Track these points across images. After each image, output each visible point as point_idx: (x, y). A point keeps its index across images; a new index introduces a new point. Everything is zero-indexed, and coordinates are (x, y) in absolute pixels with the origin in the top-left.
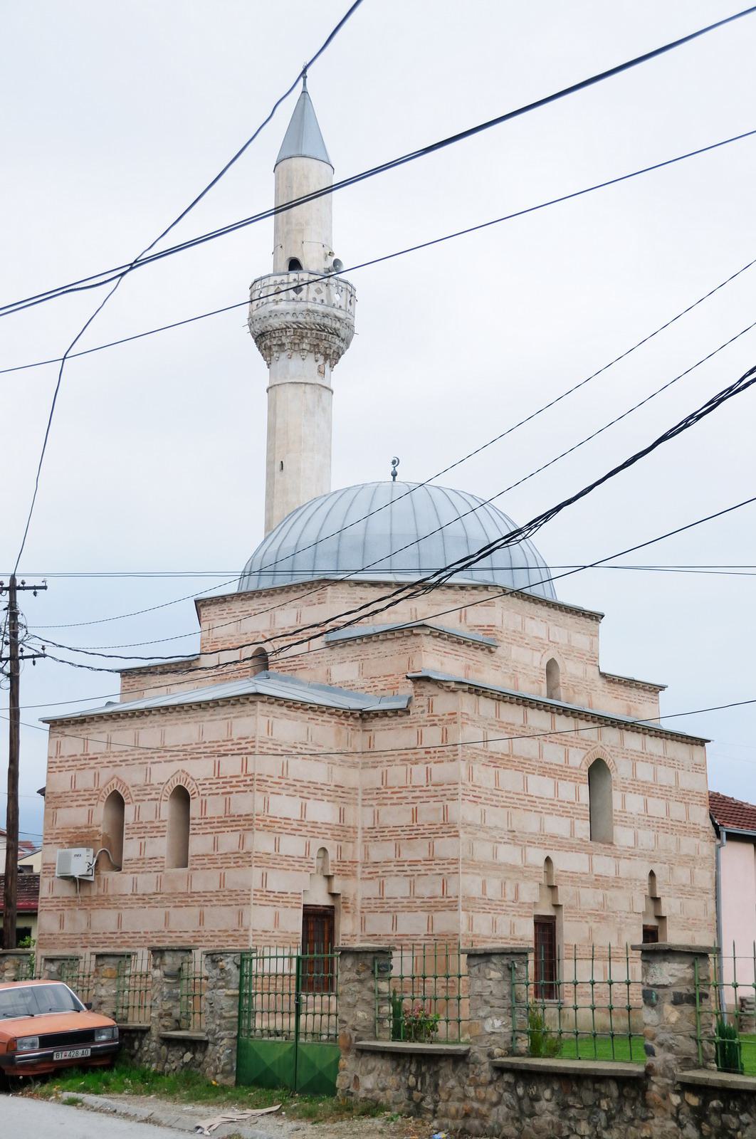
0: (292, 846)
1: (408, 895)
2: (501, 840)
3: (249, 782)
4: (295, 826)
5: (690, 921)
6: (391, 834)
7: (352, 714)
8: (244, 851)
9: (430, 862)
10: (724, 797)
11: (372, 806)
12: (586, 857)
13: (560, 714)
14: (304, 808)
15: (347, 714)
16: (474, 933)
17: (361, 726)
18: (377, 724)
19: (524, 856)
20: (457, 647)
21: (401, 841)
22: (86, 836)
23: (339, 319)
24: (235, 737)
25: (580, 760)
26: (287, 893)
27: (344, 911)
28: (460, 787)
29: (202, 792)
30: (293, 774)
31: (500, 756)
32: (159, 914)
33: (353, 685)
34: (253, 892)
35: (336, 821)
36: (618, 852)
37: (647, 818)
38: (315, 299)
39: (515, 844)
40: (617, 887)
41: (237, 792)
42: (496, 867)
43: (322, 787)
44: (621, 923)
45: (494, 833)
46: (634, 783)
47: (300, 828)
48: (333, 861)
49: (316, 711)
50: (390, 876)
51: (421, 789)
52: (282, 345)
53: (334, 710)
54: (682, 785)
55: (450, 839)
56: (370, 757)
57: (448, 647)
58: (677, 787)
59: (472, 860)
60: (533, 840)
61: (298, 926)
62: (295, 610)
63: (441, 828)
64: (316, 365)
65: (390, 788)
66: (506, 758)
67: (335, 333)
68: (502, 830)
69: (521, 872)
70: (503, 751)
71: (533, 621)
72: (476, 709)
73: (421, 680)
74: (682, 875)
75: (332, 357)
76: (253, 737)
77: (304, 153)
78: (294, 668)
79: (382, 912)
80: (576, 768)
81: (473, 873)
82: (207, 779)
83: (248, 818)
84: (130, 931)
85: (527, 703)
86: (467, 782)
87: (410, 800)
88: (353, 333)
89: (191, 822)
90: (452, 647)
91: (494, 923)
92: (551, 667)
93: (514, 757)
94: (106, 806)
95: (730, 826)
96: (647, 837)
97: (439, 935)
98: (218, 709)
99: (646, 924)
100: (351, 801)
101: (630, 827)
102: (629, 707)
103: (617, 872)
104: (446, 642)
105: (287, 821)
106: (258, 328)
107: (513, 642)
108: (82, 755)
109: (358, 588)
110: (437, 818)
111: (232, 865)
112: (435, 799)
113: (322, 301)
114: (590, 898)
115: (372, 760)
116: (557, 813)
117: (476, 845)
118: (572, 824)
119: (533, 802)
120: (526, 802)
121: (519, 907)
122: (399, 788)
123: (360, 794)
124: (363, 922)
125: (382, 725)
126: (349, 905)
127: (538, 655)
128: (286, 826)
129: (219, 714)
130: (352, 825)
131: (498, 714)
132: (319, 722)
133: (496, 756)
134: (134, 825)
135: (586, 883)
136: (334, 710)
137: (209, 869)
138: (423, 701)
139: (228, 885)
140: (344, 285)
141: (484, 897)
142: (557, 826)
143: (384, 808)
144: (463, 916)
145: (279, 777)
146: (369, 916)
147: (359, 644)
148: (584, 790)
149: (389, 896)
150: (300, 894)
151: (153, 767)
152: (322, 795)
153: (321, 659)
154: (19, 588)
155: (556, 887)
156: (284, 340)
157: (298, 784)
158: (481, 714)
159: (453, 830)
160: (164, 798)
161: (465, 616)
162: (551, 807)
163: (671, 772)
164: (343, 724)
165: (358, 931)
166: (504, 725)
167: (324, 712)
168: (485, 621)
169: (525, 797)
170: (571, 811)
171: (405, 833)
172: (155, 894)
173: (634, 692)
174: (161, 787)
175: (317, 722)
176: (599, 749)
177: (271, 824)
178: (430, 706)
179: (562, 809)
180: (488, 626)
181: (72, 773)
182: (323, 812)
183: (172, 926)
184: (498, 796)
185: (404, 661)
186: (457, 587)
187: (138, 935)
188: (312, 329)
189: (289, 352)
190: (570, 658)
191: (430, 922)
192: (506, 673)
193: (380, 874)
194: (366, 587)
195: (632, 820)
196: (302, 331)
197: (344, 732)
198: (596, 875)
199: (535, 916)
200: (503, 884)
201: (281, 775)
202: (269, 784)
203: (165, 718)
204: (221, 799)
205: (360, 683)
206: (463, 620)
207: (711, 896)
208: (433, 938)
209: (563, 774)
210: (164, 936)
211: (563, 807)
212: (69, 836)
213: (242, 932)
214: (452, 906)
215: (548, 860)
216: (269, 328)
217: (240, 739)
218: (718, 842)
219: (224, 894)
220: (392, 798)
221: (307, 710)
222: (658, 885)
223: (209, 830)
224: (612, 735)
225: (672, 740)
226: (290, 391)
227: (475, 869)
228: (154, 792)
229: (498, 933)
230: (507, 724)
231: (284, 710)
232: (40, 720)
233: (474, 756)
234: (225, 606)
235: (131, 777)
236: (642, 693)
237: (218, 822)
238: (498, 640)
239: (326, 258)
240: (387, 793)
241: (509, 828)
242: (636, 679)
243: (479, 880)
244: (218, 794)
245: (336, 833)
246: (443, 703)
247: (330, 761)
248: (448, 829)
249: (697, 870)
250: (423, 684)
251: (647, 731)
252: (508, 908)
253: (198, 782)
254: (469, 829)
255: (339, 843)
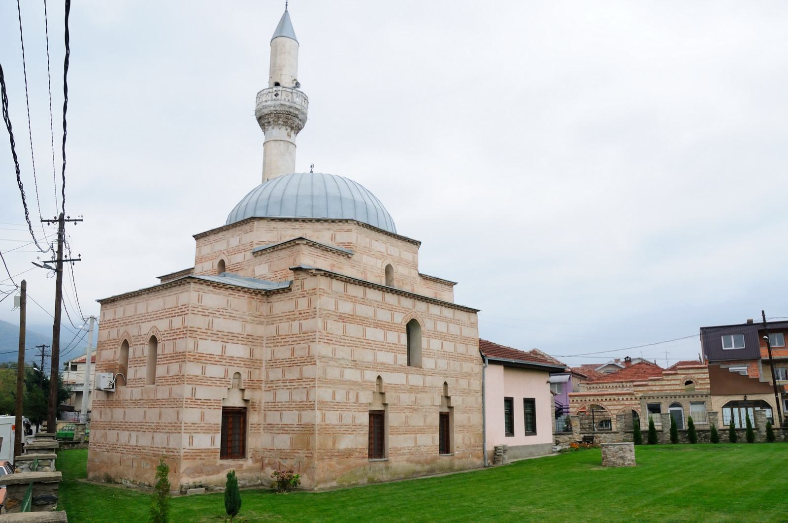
0: (215, 371)
1: (288, 400)
2: (346, 366)
3: (188, 332)
4: (217, 359)
5: (468, 408)
6: (280, 363)
7: (259, 292)
8: (181, 374)
9: (300, 380)
10: (491, 343)
11: (271, 347)
12: (404, 375)
13: (388, 292)
14: (224, 349)
15: (257, 292)
16: (326, 423)
17: (266, 300)
18: (274, 298)
19: (362, 376)
20: (325, 253)
21: (285, 368)
22: (112, 366)
23: (298, 109)
24: (180, 305)
25: (401, 320)
26: (210, 400)
27: (252, 410)
28: (318, 333)
29: (163, 339)
30: (216, 327)
31: (346, 316)
32: (141, 411)
33: (266, 277)
34: (185, 400)
35: (248, 356)
36: (425, 372)
37: (443, 353)
38: (285, 99)
39: (356, 369)
40: (424, 392)
41: (179, 338)
42: (342, 382)
43: (238, 335)
44: (426, 412)
45: (342, 362)
46: (435, 333)
47: (221, 360)
48: (245, 380)
49: (234, 290)
50: (279, 389)
51: (296, 336)
52: (269, 122)
53: (246, 290)
54: (464, 334)
55: (311, 366)
56: (271, 319)
57: (319, 252)
58: (461, 335)
59: (326, 379)
60: (369, 366)
61: (219, 420)
62: (239, 237)
63: (307, 359)
64: (287, 132)
65: (280, 336)
66: (351, 317)
67: (296, 116)
68: (348, 360)
69: (361, 385)
70: (349, 313)
71: (377, 243)
72: (330, 287)
73: (298, 270)
74: (463, 383)
75: (298, 129)
76: (188, 304)
77: (283, 35)
78: (237, 269)
79: (275, 411)
80: (398, 324)
81: (326, 387)
82: (165, 331)
83: (183, 354)
84: (129, 421)
85: (366, 285)
86: (323, 331)
87: (291, 343)
88: (307, 117)
89: (158, 357)
90: (323, 253)
91: (341, 417)
92: (388, 270)
93: (357, 316)
94: (121, 349)
95: (490, 356)
96: (442, 364)
97: (304, 425)
98: (173, 288)
99: (441, 411)
100: (258, 344)
101: (432, 358)
102: (436, 293)
103: (424, 383)
104: (318, 249)
105: (211, 356)
106: (259, 115)
107: (363, 253)
108: (113, 320)
109: (273, 222)
110: (304, 353)
111: (175, 383)
112: (303, 342)
113: (289, 100)
114: (406, 399)
115: (271, 319)
116: (385, 350)
117: (328, 369)
118: (396, 356)
119: (369, 343)
120: (364, 344)
121: (359, 406)
122: (285, 335)
123: (265, 340)
124: (265, 416)
125: (278, 299)
126: (256, 406)
127: (380, 262)
128: (210, 359)
129: (173, 292)
130: (259, 358)
131: (345, 290)
132: (236, 296)
133: (343, 315)
134: (133, 360)
135: (405, 390)
136: (246, 290)
137: (165, 385)
138: (298, 283)
139: (173, 395)
140: (301, 94)
141: (333, 401)
142: (386, 357)
143: (276, 348)
144: (318, 413)
145: (206, 329)
146: (269, 413)
147: (269, 253)
148: (404, 337)
149: (279, 401)
150: (220, 400)
151: (142, 325)
152: (238, 340)
153: (250, 264)
154: (66, 220)
155: (384, 393)
156: (271, 120)
157: (220, 334)
158: (333, 289)
159: (313, 360)
160: (146, 343)
161: (335, 237)
162: (381, 346)
163: (458, 327)
164: (254, 298)
165: (262, 422)
166: (350, 297)
167: (239, 291)
168: (346, 240)
169: (364, 341)
170: (395, 349)
171: (287, 363)
172: (141, 400)
173: (439, 285)
174: (145, 336)
175: (235, 296)
176: (413, 313)
177: (199, 358)
178: (302, 285)
179: (388, 348)
180: (348, 243)
181: (108, 330)
182: (238, 351)
183: (147, 419)
184: (345, 340)
185: (292, 260)
186: (330, 221)
187: (132, 424)
188: (284, 114)
189: (272, 126)
190: (400, 264)
191: (300, 416)
192: (359, 270)
193: (274, 387)
194: (277, 222)
195: (434, 354)
196: (281, 117)
197: (254, 303)
198: (410, 386)
199: (369, 411)
200: (348, 393)
201: (207, 328)
202: (198, 333)
203: (149, 296)
204: (171, 342)
205: (268, 276)
206: (333, 240)
207: (480, 394)
208: (301, 427)
209: (389, 327)
210: (143, 425)
211: (390, 346)
212: (106, 366)
213: (179, 425)
214: (311, 408)
215: (379, 378)
216: (263, 114)
217: (182, 306)
218: (484, 365)
219: (171, 400)
220: (281, 342)
221: (227, 289)
222: (449, 390)
223: (166, 362)
224: (422, 306)
225: (458, 310)
226: (273, 144)
227: (328, 384)
228: (142, 340)
229: (343, 422)
230: (352, 296)
231: (211, 288)
232: (96, 301)
233: (328, 315)
234: (206, 238)
235: (133, 331)
236: (444, 286)
237: (170, 357)
238: (354, 251)
239: (293, 82)
240: (278, 339)
241: (353, 359)
242: (440, 278)
243: (330, 391)
244: (170, 340)
245: (247, 363)
246: (310, 283)
247: (243, 320)
248: (310, 360)
249: (472, 381)
250: (299, 272)
251: (443, 304)
252: (351, 407)
253: (162, 333)
254: (323, 360)
255: (250, 370)
